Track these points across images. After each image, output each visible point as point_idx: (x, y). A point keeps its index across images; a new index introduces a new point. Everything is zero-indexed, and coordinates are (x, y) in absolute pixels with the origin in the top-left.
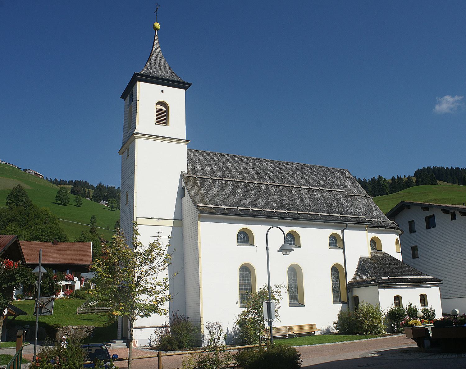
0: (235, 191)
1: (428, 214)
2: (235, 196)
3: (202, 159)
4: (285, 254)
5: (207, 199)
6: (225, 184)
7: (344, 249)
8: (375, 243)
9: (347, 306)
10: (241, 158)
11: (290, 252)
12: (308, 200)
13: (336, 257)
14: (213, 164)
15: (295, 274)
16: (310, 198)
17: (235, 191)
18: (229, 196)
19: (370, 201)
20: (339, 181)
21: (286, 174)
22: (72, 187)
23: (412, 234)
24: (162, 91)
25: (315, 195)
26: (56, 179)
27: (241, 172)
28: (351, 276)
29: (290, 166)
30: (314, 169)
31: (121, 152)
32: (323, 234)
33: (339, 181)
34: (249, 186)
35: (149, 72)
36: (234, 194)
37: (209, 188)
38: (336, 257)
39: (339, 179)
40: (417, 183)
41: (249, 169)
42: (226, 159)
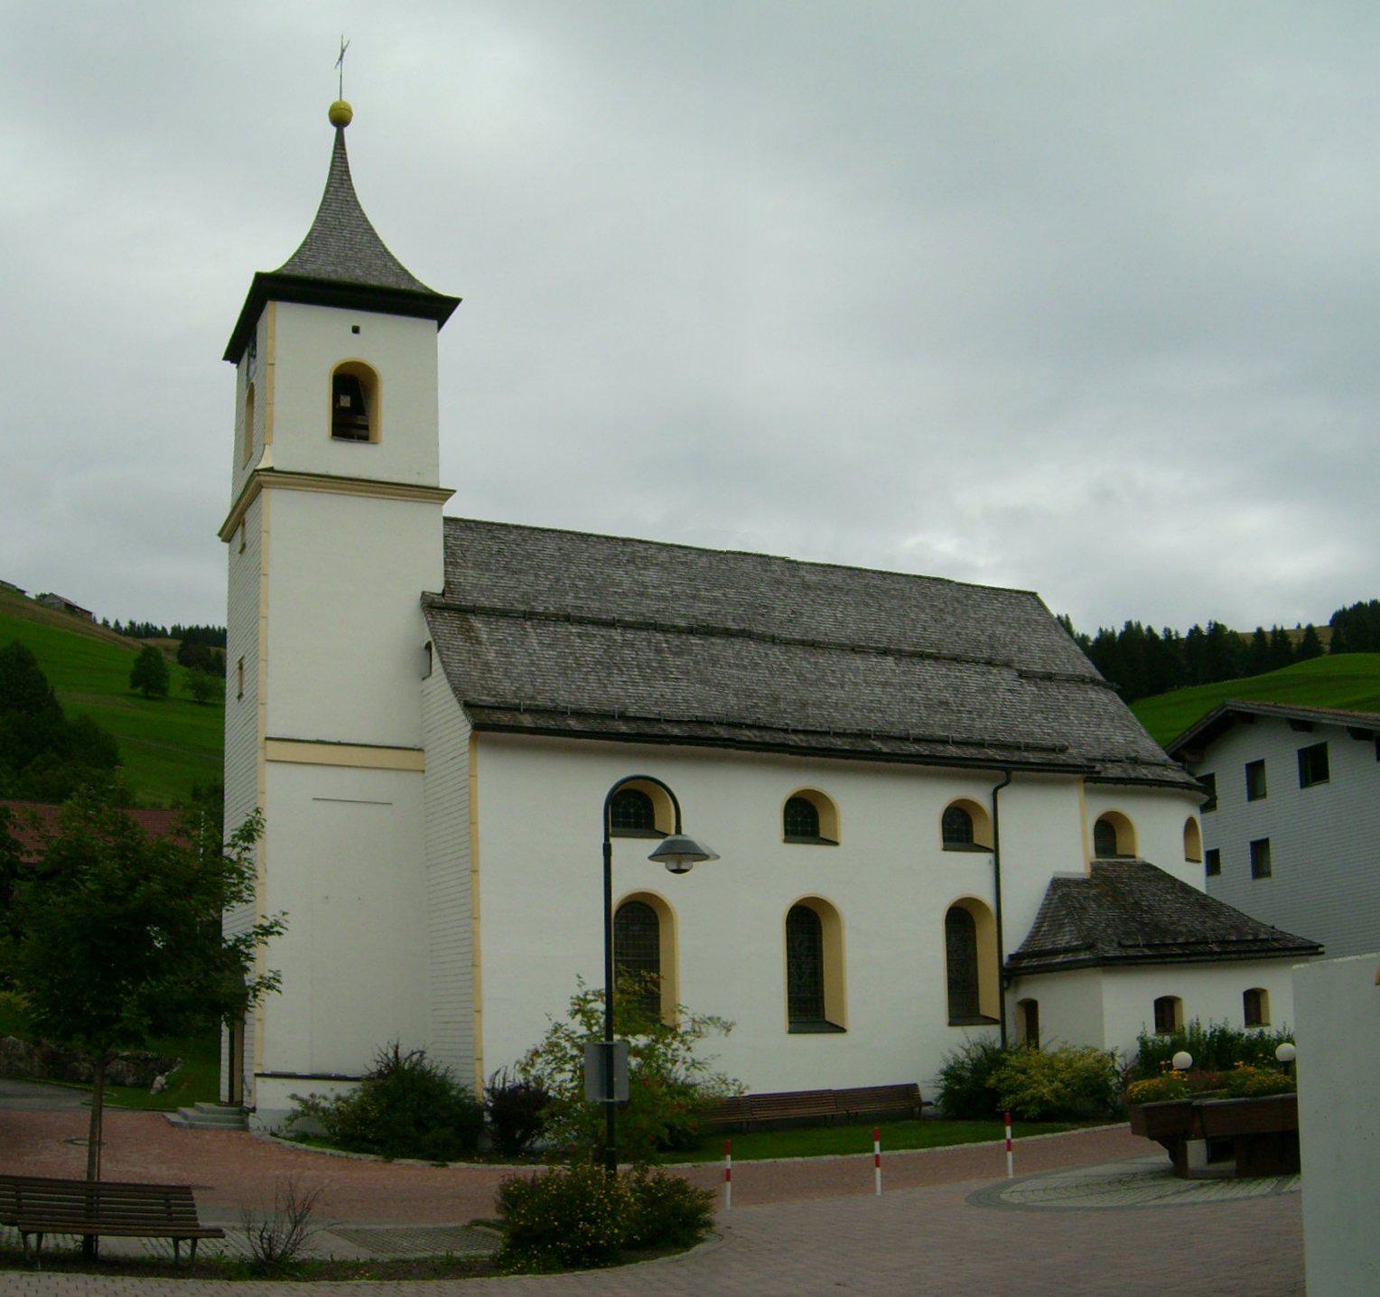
0: (611, 658)
1: (1308, 741)
2: (610, 674)
3: (500, 552)
4: (675, 867)
5: (507, 683)
6: (579, 635)
7: (995, 851)
8: (1108, 832)
9: (1000, 1031)
10: (646, 550)
11: (694, 863)
12: (878, 690)
13: (966, 875)
14: (540, 567)
15: (808, 927)
16: (885, 684)
17: (611, 658)
18: (587, 673)
19: (1107, 700)
20: (1000, 630)
21: (806, 603)
22: (181, 645)
23: (1257, 804)
24: (356, 330)
25: (904, 672)
26: (132, 624)
27: (694, 597)
28: (1016, 934)
29: (824, 577)
30: (911, 588)
31: (227, 534)
32: (923, 804)
33: (1000, 630)
34: (667, 641)
35: (308, 266)
36: (608, 668)
37: (519, 647)
38: (966, 875)
39: (1003, 623)
40: (1337, 647)
41: (675, 583)
42: (593, 551)
